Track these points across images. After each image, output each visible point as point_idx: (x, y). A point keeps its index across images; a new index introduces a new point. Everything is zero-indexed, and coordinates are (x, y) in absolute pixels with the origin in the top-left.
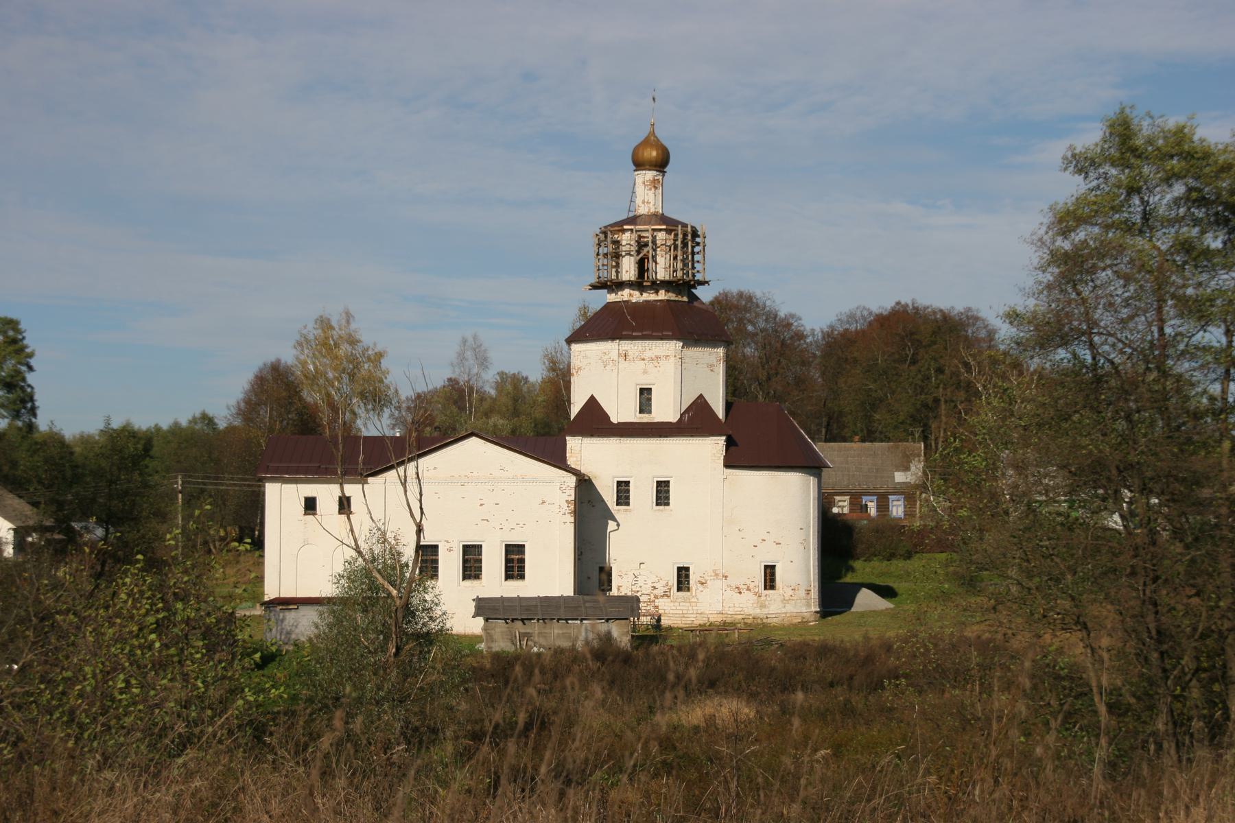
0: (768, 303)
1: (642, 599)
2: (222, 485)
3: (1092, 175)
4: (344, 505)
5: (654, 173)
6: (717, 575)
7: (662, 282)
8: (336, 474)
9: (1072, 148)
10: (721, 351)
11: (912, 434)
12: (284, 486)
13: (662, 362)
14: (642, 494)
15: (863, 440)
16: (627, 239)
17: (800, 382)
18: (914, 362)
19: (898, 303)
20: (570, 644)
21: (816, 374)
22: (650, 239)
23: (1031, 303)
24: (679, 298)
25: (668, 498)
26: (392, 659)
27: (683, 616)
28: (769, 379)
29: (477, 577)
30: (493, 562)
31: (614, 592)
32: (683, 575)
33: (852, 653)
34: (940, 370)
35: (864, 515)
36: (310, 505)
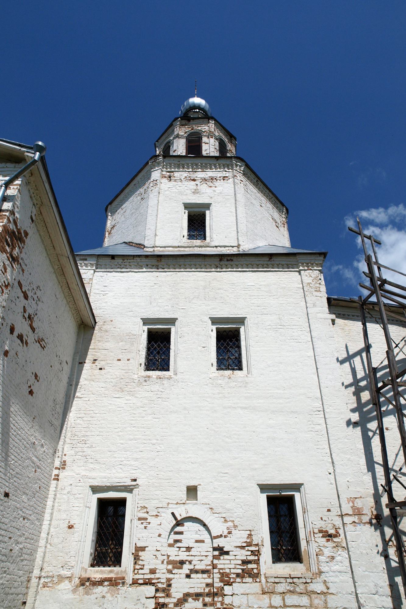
13: (217, 183)
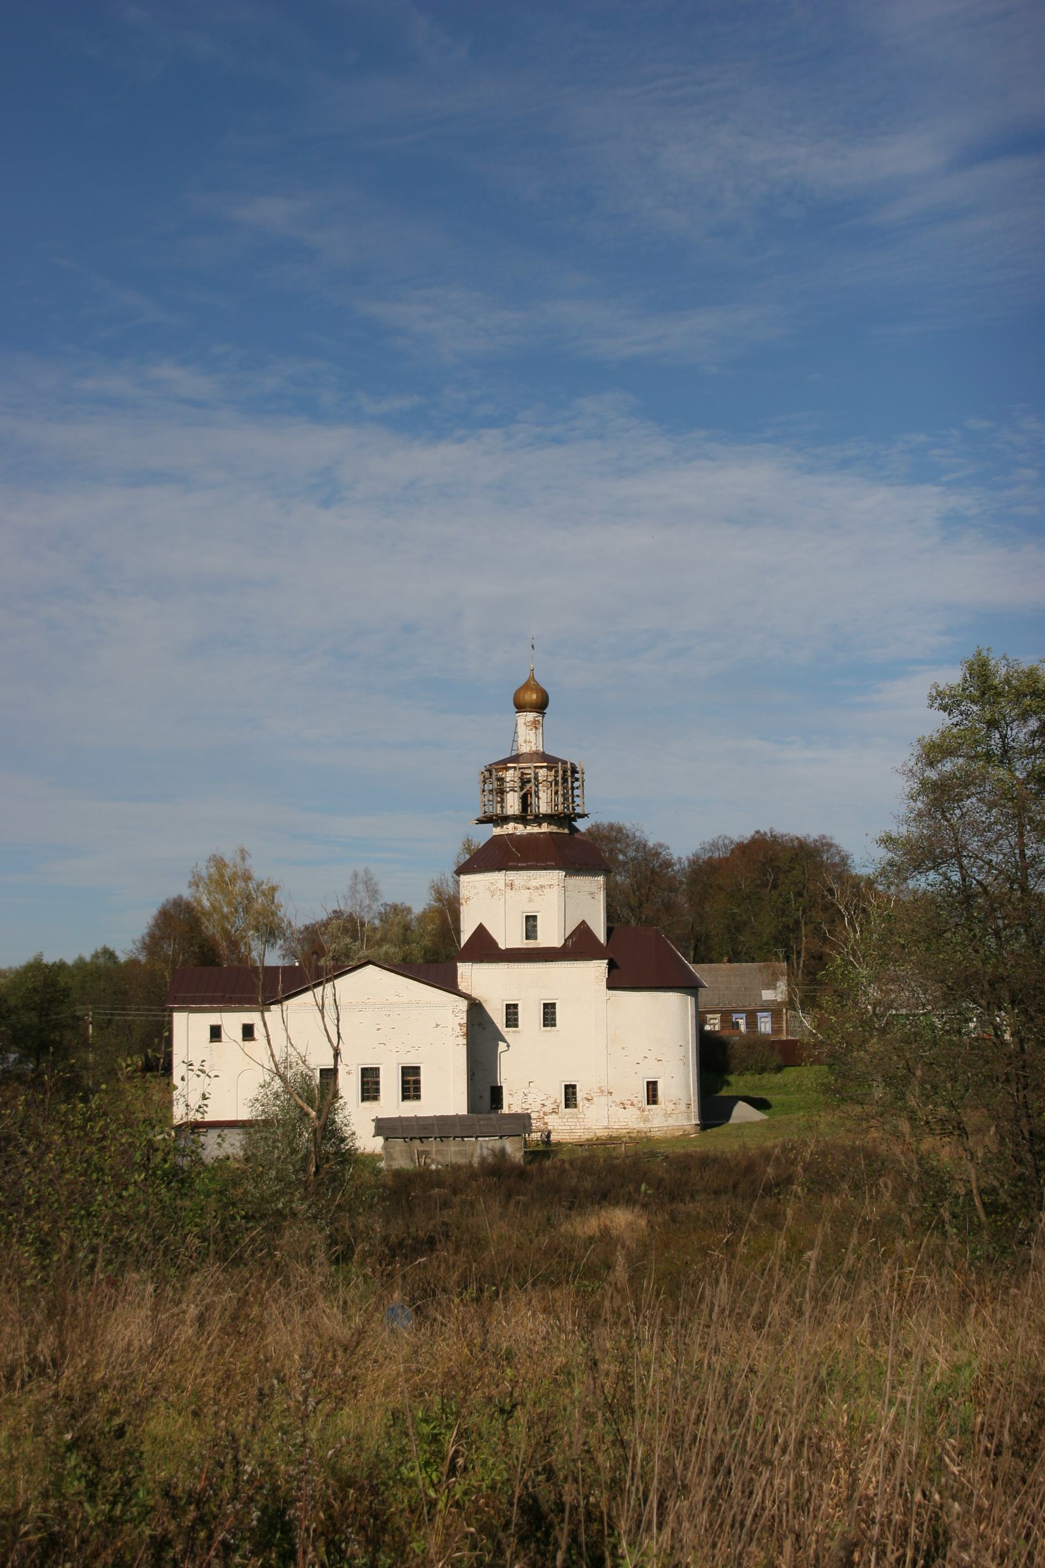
0: (637, 834)
1: (533, 1115)
2: (129, 1015)
3: (956, 712)
4: (248, 1032)
5: (535, 714)
6: (602, 1091)
7: (544, 815)
8: (257, 1003)
9: (936, 686)
10: (601, 879)
11: (776, 954)
12: (192, 1015)
14: (530, 1016)
15: (729, 961)
16: (510, 776)
17: (669, 907)
18: (775, 887)
19: (757, 832)
20: (467, 1161)
21: (682, 900)
22: (532, 776)
23: (903, 830)
24: (561, 831)
25: (554, 1019)
26: (312, 1178)
27: (571, 1131)
28: (641, 905)
29: (376, 1098)
30: (390, 1084)
31: (505, 1110)
32: (570, 1091)
33: (733, 1163)
34: (799, 894)
35: (736, 1031)
36: (216, 1033)
